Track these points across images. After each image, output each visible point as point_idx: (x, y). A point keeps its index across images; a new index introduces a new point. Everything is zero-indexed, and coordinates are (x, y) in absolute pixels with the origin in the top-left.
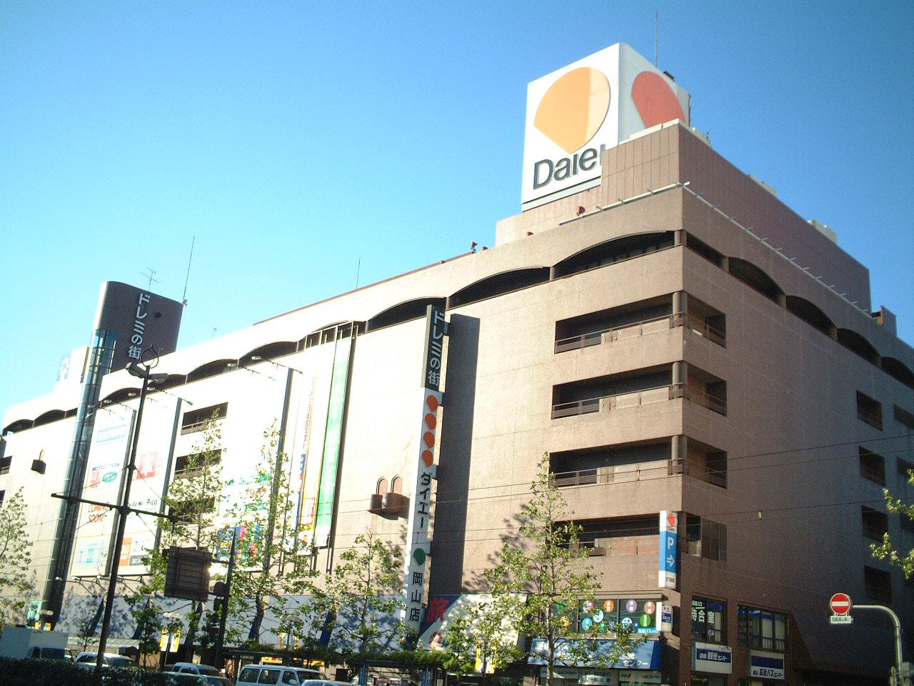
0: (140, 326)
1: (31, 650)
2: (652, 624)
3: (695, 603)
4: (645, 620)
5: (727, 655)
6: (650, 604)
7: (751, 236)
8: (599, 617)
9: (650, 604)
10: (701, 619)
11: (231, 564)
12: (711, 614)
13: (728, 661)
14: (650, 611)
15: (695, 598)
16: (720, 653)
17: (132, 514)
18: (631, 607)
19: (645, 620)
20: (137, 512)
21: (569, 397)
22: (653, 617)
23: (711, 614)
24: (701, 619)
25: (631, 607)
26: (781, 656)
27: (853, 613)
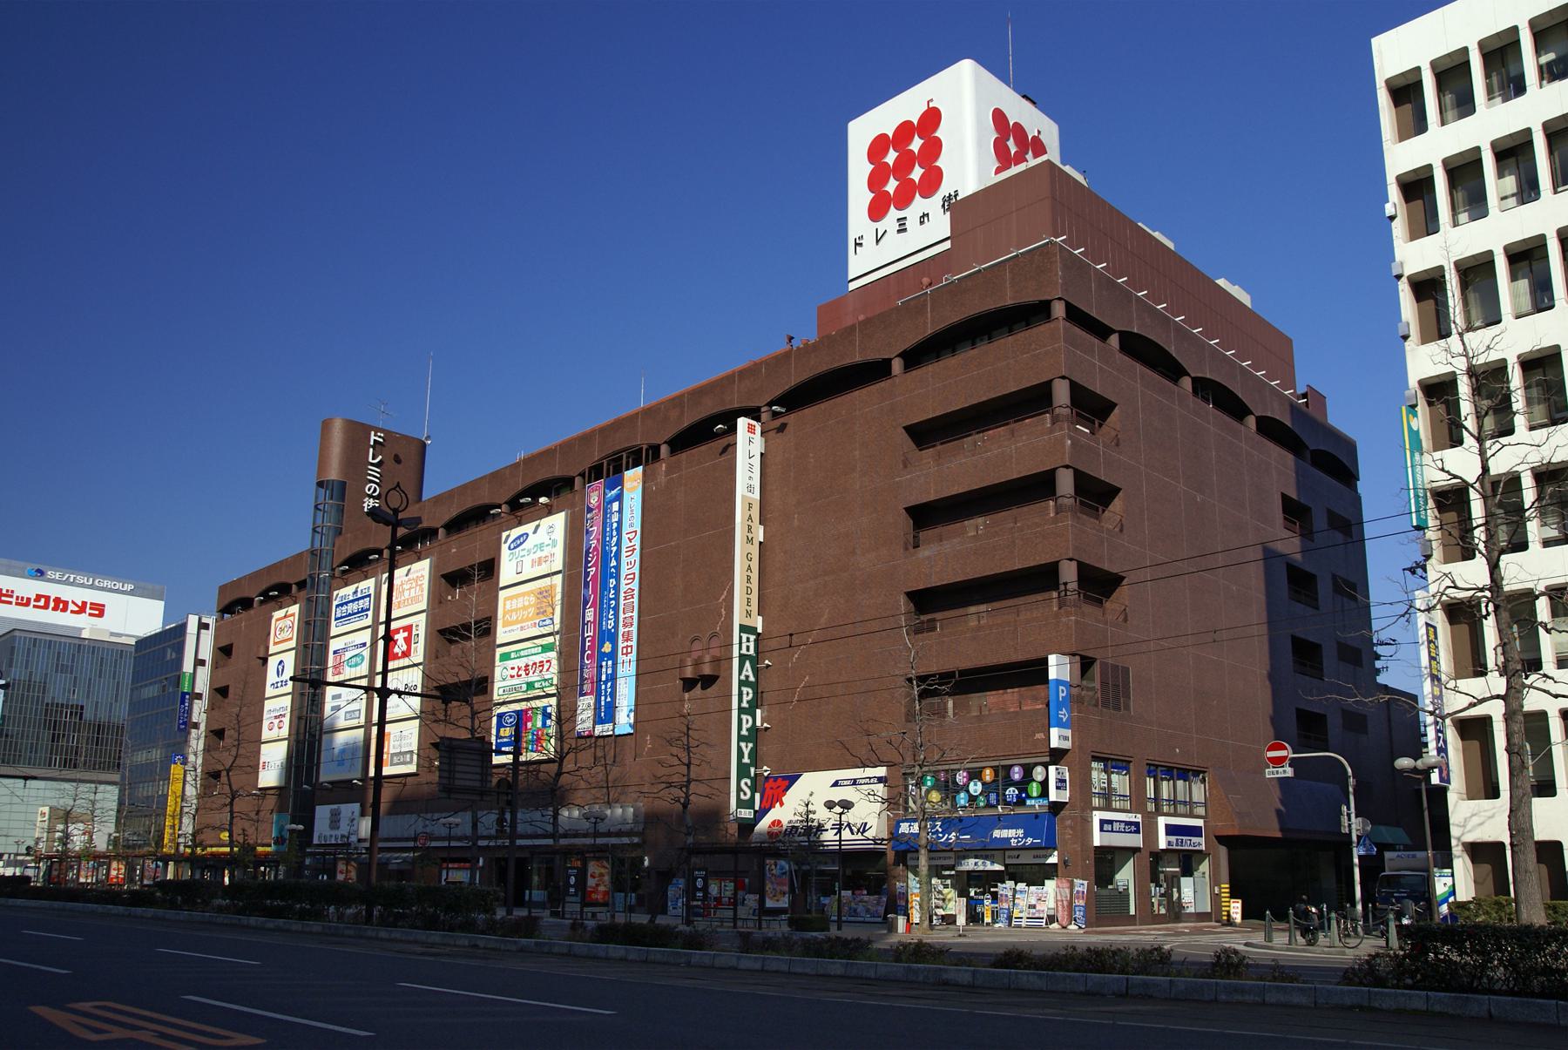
0: (374, 472)
1: (1082, 503)
2: (1044, 793)
3: (1094, 765)
4: (1034, 789)
5: (1136, 824)
6: (1039, 769)
7: (151, 1010)
8: (976, 788)
9: (1039, 769)
10: (335, 821)
11: (517, 753)
12: (1114, 777)
13: (1137, 832)
14: (1040, 778)
15: (1096, 759)
16: (1127, 823)
17: (394, 697)
18: (1017, 774)
19: (1034, 789)
20: (400, 693)
21: (925, 516)
22: (1044, 784)
23: (1114, 777)
24: (335, 821)
25: (1017, 774)
26: (1199, 823)
27: (1293, 762)
